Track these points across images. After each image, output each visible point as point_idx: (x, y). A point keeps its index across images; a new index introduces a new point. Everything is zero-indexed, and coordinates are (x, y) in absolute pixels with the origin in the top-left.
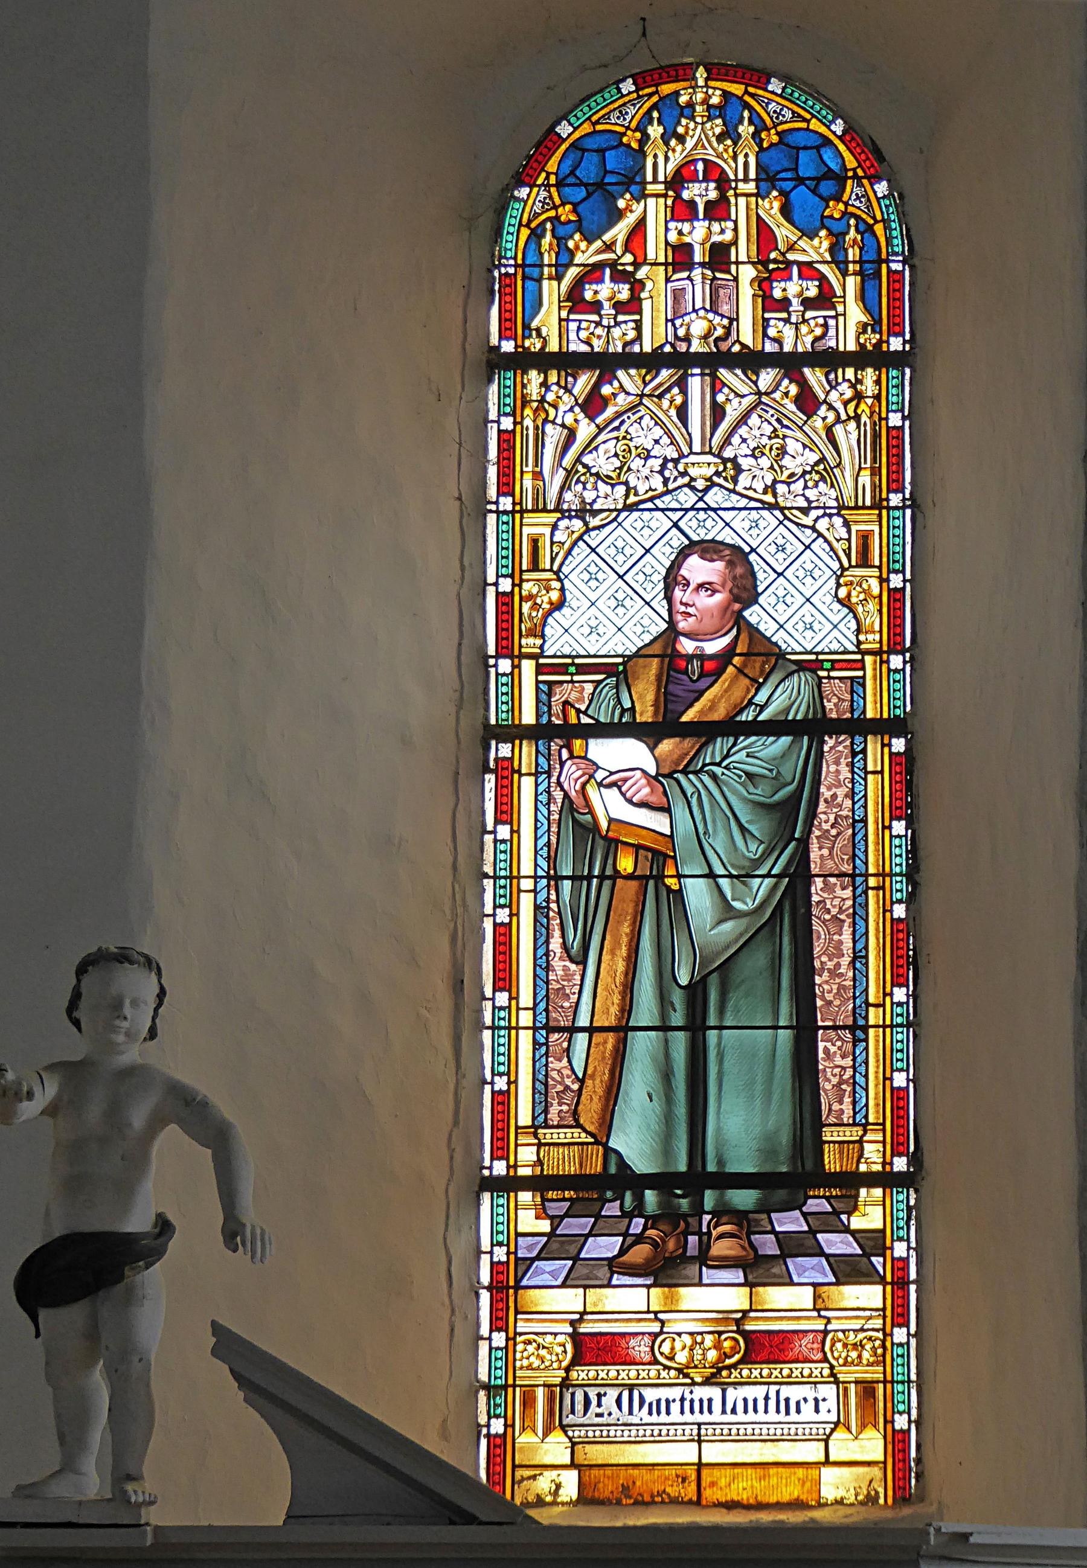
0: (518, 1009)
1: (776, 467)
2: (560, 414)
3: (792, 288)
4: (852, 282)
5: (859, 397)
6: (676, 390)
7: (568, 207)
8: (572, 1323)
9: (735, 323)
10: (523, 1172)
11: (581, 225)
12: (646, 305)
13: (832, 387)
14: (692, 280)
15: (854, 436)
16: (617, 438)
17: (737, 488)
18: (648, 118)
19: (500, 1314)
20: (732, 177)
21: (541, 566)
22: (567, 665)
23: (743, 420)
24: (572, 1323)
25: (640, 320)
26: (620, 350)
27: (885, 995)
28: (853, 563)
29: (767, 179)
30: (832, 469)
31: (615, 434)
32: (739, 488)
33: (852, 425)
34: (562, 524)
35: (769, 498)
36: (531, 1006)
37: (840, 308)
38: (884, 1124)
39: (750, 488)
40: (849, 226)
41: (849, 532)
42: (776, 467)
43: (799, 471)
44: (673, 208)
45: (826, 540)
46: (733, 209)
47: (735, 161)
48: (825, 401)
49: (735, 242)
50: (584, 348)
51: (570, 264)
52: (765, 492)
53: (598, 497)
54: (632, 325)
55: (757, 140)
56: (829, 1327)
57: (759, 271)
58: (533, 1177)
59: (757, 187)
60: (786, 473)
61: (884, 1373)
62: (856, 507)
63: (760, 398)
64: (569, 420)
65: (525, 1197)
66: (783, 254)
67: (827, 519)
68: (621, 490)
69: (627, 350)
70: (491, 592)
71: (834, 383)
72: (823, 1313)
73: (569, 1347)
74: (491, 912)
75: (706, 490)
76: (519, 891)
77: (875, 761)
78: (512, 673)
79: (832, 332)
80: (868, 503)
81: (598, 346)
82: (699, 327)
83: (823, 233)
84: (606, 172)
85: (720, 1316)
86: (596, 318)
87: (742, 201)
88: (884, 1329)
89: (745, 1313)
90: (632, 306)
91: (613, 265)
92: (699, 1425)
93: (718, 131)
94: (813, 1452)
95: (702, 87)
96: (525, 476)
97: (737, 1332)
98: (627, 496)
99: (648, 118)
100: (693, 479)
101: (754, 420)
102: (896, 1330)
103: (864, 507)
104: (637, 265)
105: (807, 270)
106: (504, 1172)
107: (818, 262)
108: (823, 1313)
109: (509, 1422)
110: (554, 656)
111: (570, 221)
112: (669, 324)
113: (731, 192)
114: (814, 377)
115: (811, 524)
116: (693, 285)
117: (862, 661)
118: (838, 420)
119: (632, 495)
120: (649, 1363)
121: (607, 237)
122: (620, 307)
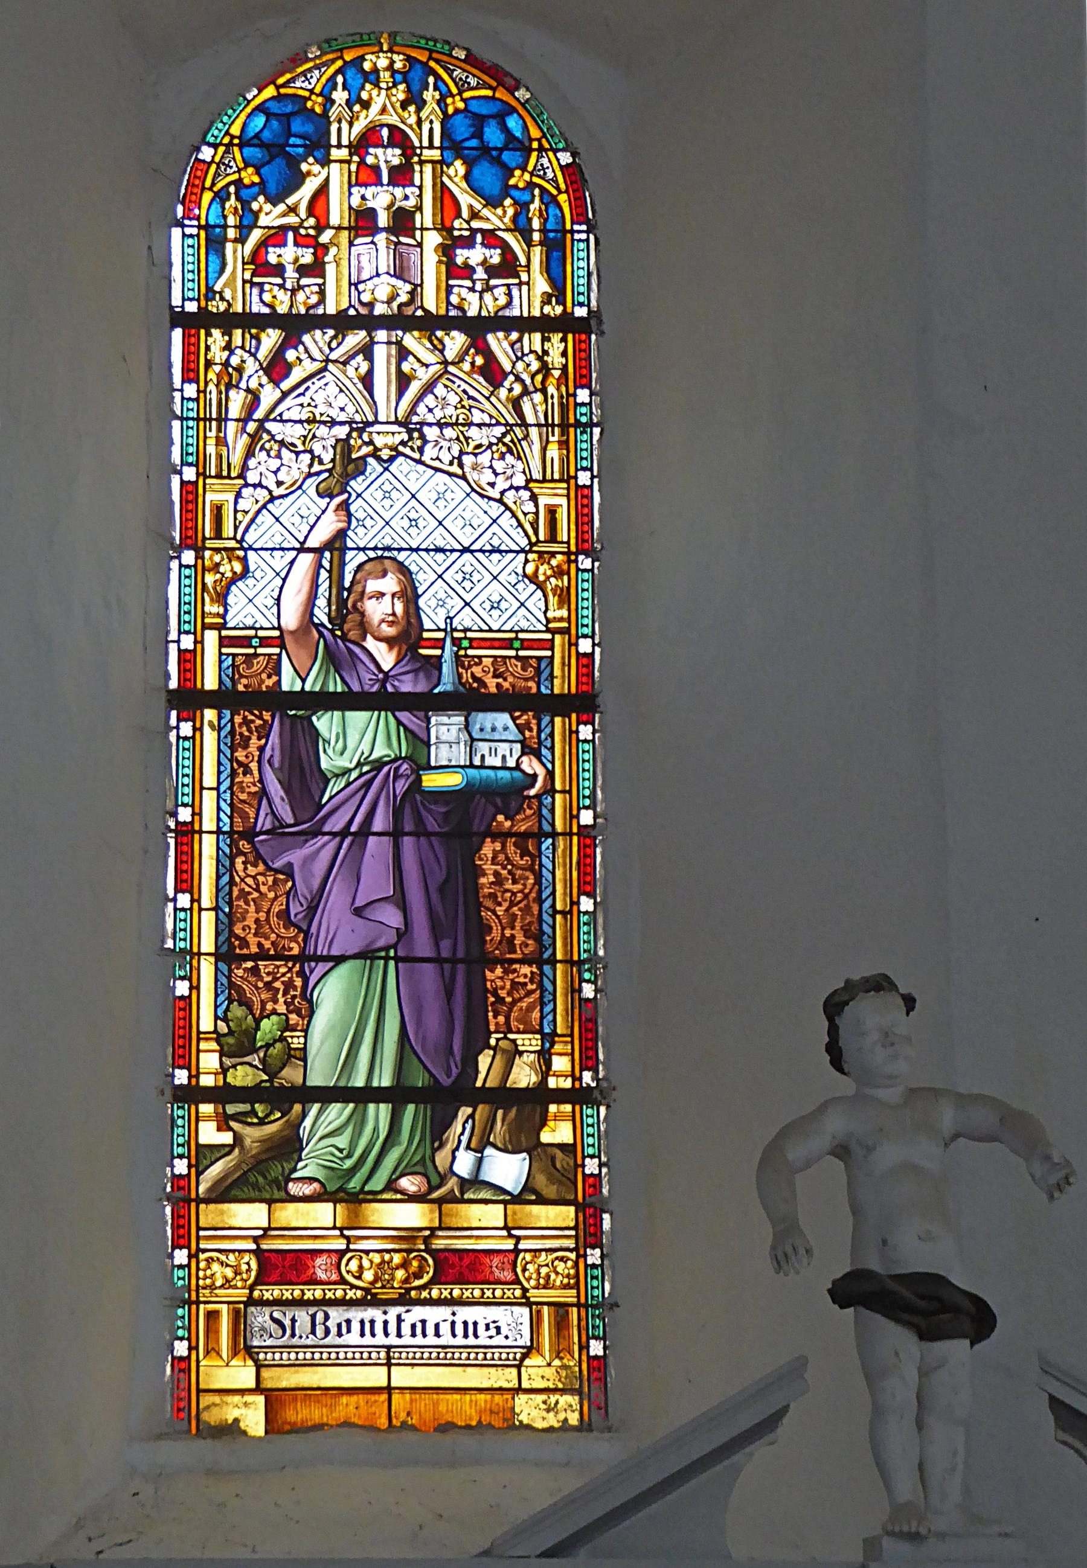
0: (200, 910)
1: (462, 438)
2: (245, 378)
3: (475, 255)
4: (537, 253)
5: (545, 369)
6: (360, 357)
7: (250, 170)
8: (256, 1239)
9: (419, 289)
10: (207, 1081)
11: (265, 187)
12: (330, 270)
13: (518, 358)
14: (375, 245)
15: (541, 409)
16: (302, 405)
17: (423, 459)
18: (332, 83)
19: (188, 666)
20: (417, 144)
21: (225, 535)
22: (250, 638)
23: (429, 388)
24: (256, 1239)
25: (324, 284)
26: (303, 311)
27: (572, 903)
28: (542, 538)
29: (452, 146)
30: (519, 441)
31: (301, 400)
32: (426, 458)
33: (538, 397)
34: (246, 492)
35: (455, 469)
36: (215, 785)
37: (524, 277)
38: (572, 1035)
39: (438, 458)
40: (533, 196)
41: (537, 506)
42: (462, 438)
43: (485, 442)
44: (357, 173)
45: (514, 515)
46: (417, 176)
47: (420, 128)
48: (511, 372)
49: (419, 208)
50: (266, 310)
51: (254, 225)
52: (451, 463)
53: (282, 465)
54: (316, 289)
55: (443, 105)
56: (521, 1247)
57: (444, 238)
58: (215, 1088)
59: (442, 155)
60: (472, 444)
61: (578, 1297)
62: (544, 481)
63: (446, 368)
64: (253, 384)
65: (206, 1109)
66: (468, 222)
67: (513, 491)
68: (306, 458)
69: (311, 312)
70: (173, 649)
71: (519, 354)
72: (514, 1232)
73: (254, 1265)
74: (176, 638)
75: (392, 459)
76: (202, 788)
77: (564, 782)
78: (193, 737)
79: (516, 301)
80: (556, 476)
81: (282, 309)
82: (383, 293)
83: (508, 202)
84: (290, 135)
85: (409, 1234)
86: (279, 281)
87: (428, 169)
88: (576, 1249)
89: (432, 1230)
90: (316, 269)
91: (295, 229)
92: (389, 1348)
93: (402, 96)
94: (506, 1378)
95: (386, 52)
96: (208, 441)
97: (427, 1250)
98: (311, 466)
99: (332, 83)
100: (376, 449)
101: (439, 390)
102: (582, 727)
103: (553, 481)
104: (320, 228)
105: (491, 238)
106: (185, 1082)
107: (500, 229)
108: (514, 1232)
109: (194, 1344)
110: (234, 628)
111: (253, 184)
112: (353, 288)
113: (416, 159)
114: (497, 342)
115: (498, 496)
116: (377, 250)
117: (553, 640)
118: (526, 392)
119: (316, 463)
120: (335, 1283)
121: (290, 201)
122: (303, 270)
